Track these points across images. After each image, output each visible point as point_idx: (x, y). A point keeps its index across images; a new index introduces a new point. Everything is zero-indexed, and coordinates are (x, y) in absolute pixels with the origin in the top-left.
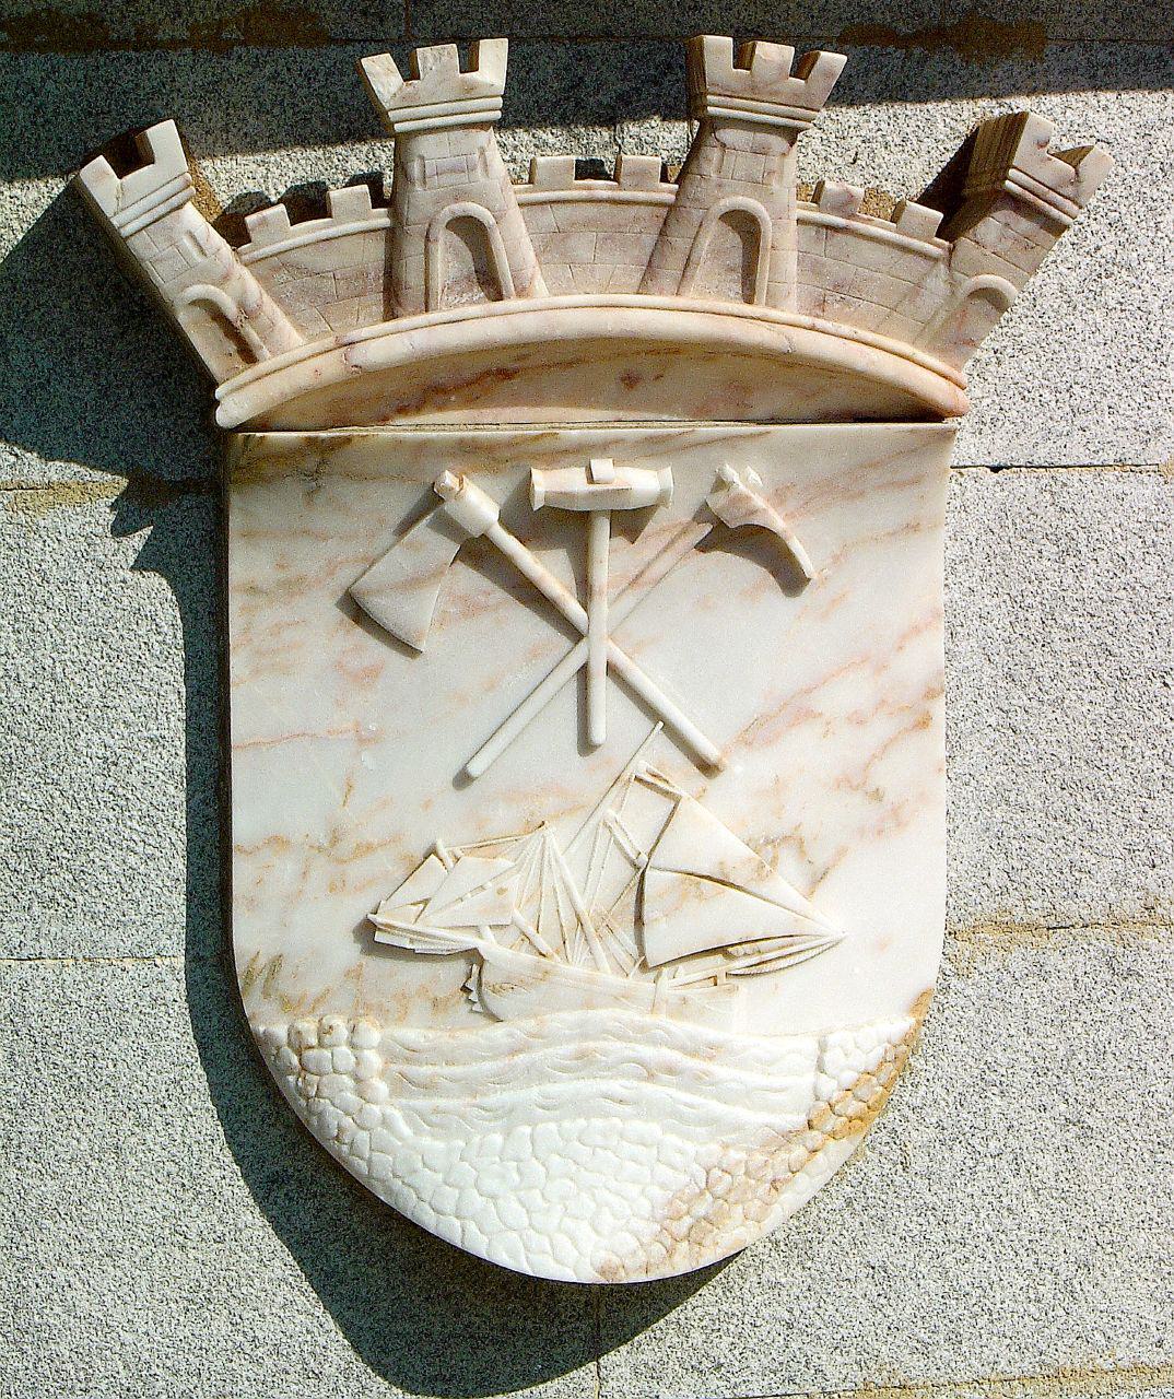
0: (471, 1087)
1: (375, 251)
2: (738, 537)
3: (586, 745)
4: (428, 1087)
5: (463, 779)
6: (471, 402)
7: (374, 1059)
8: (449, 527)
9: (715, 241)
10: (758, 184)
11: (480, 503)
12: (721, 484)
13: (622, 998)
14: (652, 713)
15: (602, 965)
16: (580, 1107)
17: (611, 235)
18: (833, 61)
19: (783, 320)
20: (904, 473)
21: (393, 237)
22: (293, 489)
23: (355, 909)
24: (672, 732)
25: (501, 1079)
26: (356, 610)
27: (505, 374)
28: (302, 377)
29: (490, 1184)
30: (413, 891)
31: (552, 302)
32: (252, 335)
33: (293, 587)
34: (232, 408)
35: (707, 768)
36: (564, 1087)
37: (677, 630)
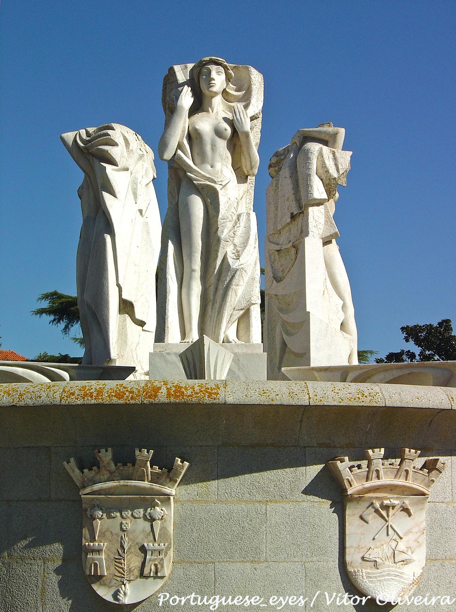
0: (376, 577)
1: (366, 473)
2: (406, 510)
3: (388, 535)
4: (371, 577)
5: (374, 539)
6: (374, 492)
7: (364, 574)
8: (374, 507)
9: (404, 473)
10: (409, 466)
11: (377, 505)
12: (404, 503)
13: (393, 567)
14: (395, 531)
15: (389, 563)
16: (388, 580)
17: (392, 472)
18: (419, 452)
19: (410, 483)
20: (422, 502)
21: (368, 472)
22: (356, 502)
23: (361, 555)
24: (397, 534)
25: (379, 576)
26: (361, 518)
27: (378, 489)
28: (358, 488)
29: (378, 590)
30: (368, 553)
31: (386, 480)
32: (352, 483)
33: (354, 515)
34: (349, 492)
35: (401, 538)
36: (387, 578)
37: (398, 521)
